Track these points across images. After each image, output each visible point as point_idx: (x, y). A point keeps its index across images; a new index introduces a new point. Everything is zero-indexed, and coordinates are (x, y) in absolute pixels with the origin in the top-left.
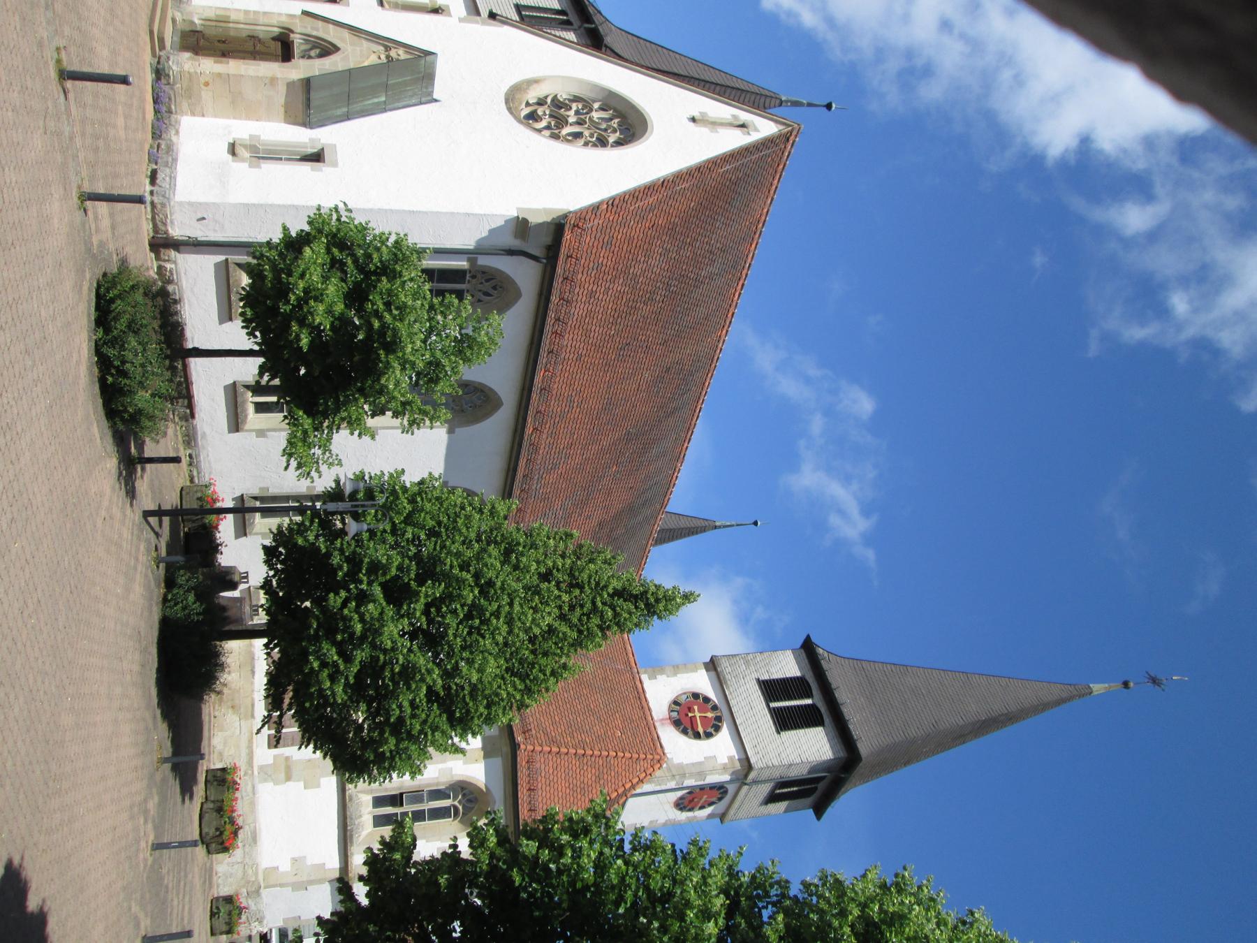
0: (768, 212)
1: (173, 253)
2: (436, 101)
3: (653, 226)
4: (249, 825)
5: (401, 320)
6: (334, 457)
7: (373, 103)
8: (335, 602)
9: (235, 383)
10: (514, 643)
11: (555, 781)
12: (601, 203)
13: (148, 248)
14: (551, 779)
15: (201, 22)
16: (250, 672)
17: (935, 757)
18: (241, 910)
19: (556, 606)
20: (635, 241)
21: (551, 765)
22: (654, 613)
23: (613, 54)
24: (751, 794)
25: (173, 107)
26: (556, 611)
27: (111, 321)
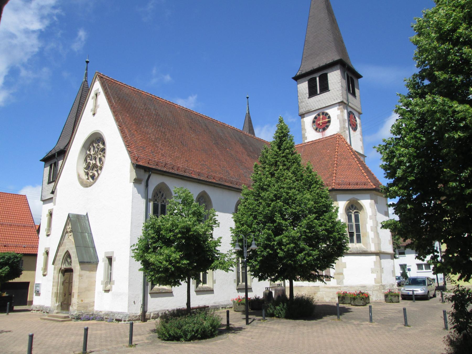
1: (147, 313)
2: (87, 214)
3: (136, 131)
4: (359, 289)
5: (178, 226)
6: (229, 253)
7: (89, 238)
8: (282, 254)
10: (298, 187)
11: (346, 175)
12: (128, 150)
13: (145, 323)
14: (345, 176)
15: (57, 303)
17: (340, 30)
18: (390, 292)
21: (340, 177)
23: (68, 146)
24: (352, 102)
25: (91, 313)
26: (192, 218)
27: (177, 335)
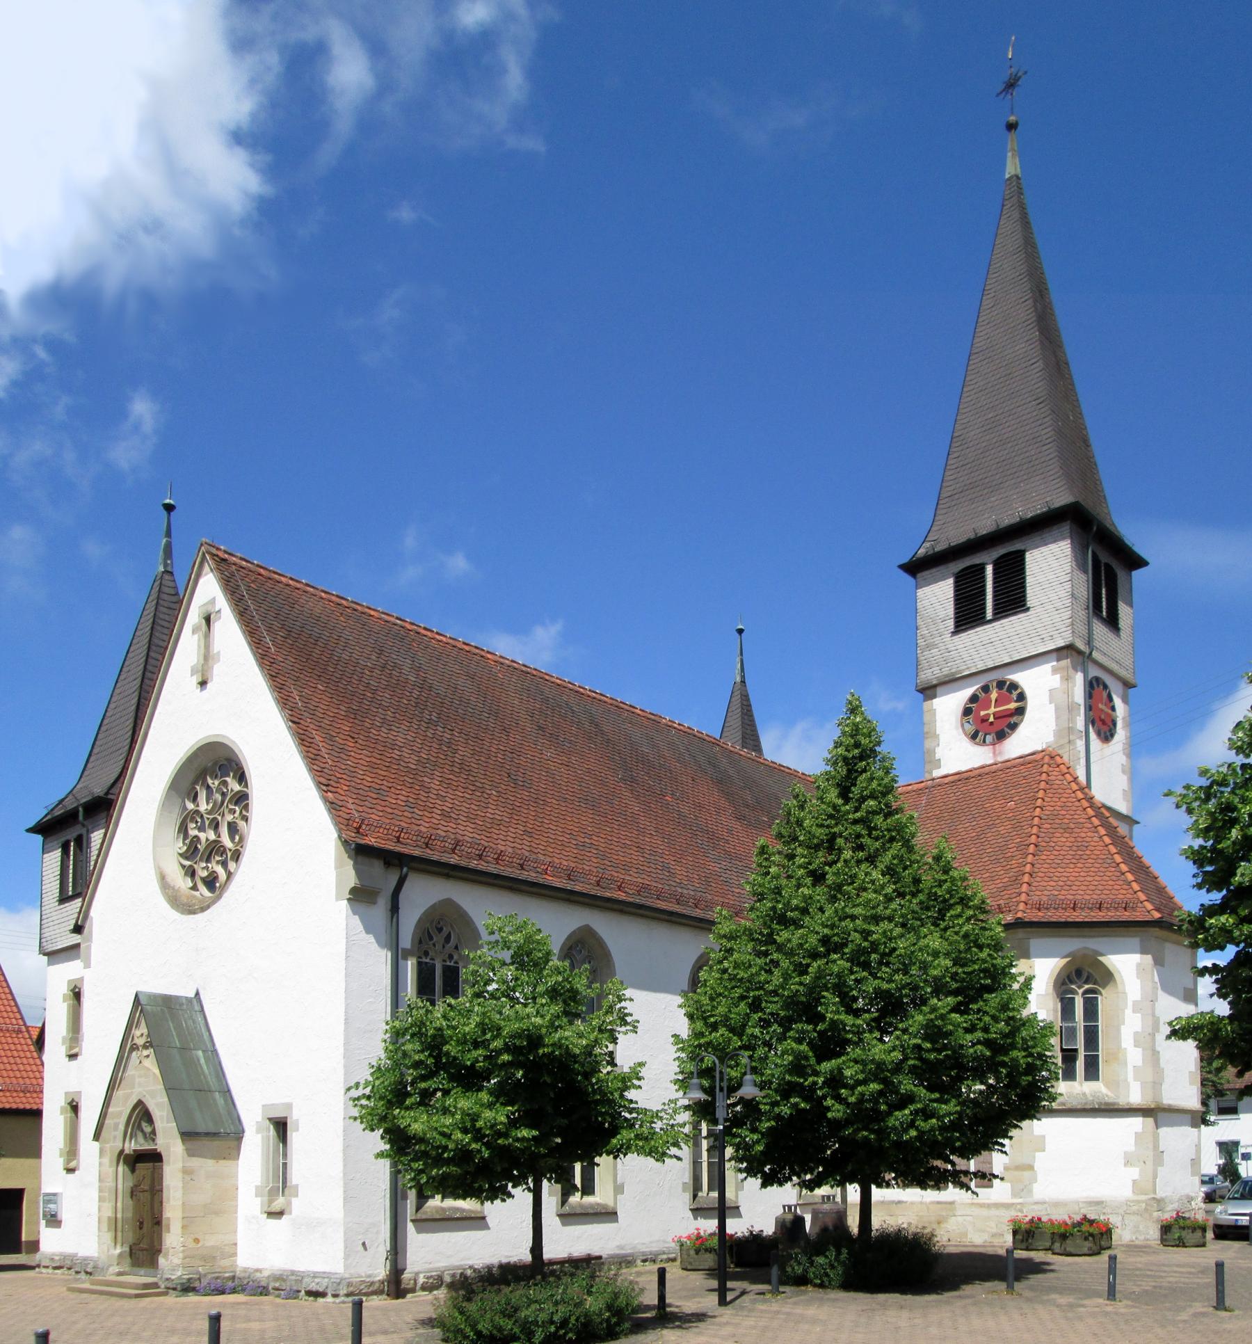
0: (325, 592)
1: (406, 1276)
2: (197, 994)
3: (353, 738)
4: (1080, 1209)
5: (499, 1029)
6: (666, 1107)
9: (558, 1215)
10: (902, 916)
12: (325, 800)
13: (400, 1301)
15: (119, 1246)
16: (899, 1205)
18: (1179, 1217)
19: (858, 866)
20: (374, 760)
21: (1045, 884)
22: (873, 751)
23: (119, 785)
24: (1104, 648)
25: (227, 1275)
26: (863, 866)
27: (502, 1334)
